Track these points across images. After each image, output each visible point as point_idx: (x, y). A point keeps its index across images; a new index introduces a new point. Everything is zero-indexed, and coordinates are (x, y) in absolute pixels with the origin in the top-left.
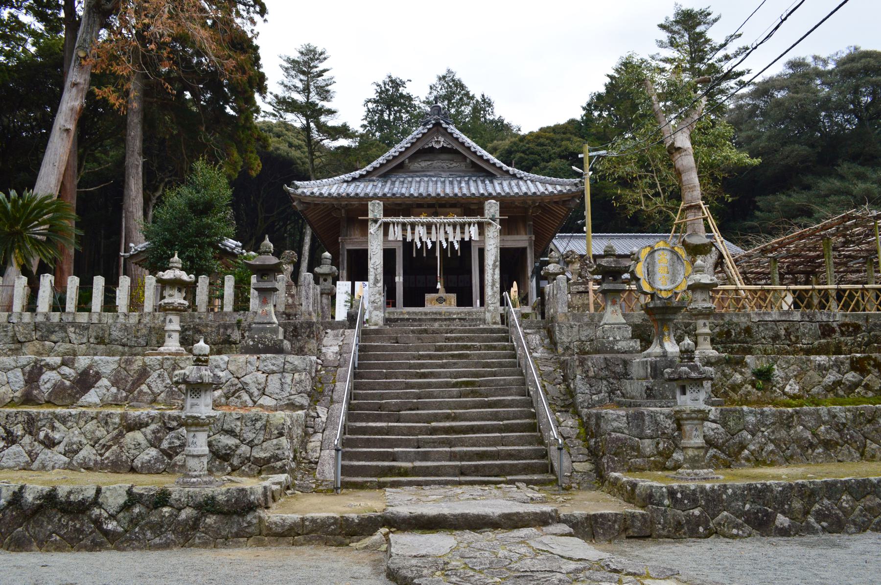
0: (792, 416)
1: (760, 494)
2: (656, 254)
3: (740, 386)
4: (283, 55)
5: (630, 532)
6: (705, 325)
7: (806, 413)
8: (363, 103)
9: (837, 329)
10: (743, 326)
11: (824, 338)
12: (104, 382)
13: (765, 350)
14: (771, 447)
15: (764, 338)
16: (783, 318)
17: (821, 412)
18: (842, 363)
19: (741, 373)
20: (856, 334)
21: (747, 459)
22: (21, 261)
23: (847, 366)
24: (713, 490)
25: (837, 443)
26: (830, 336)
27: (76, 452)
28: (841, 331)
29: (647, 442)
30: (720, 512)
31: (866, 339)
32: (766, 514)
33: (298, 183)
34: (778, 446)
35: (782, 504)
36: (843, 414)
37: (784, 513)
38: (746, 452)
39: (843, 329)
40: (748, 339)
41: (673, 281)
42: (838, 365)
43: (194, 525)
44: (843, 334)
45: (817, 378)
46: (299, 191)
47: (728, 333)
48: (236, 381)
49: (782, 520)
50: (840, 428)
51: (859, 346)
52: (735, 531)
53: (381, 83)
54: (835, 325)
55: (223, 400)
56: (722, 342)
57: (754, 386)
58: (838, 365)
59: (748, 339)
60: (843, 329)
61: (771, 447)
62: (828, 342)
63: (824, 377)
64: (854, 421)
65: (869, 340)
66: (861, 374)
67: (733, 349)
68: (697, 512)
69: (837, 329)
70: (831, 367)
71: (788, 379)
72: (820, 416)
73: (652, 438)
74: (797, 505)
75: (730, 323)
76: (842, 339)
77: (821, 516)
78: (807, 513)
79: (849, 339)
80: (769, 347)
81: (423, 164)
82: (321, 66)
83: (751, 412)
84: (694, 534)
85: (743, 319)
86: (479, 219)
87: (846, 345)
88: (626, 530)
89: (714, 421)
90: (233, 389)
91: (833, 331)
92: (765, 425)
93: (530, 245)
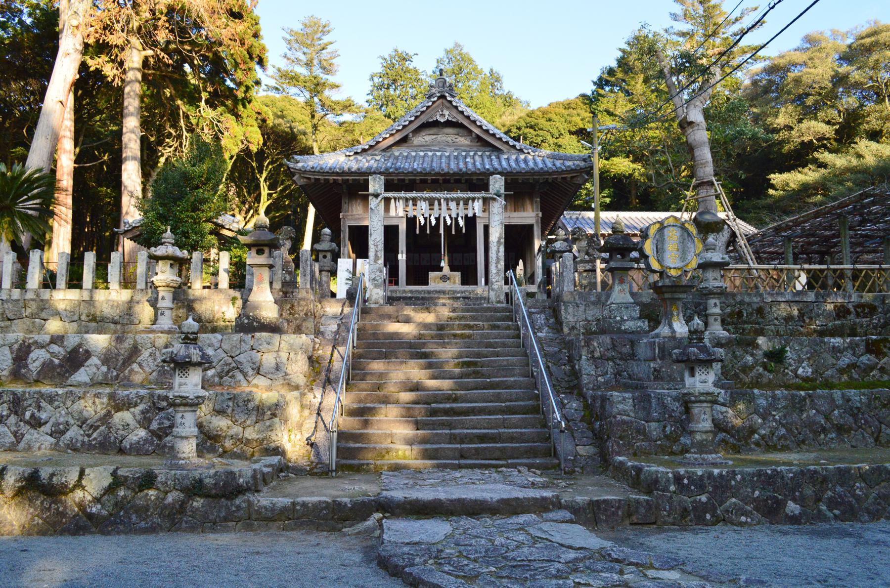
0: (804, 399)
1: (769, 480)
2: (666, 231)
3: (752, 368)
4: (286, 27)
5: (634, 519)
6: (715, 305)
7: (820, 397)
8: (368, 77)
9: (852, 310)
10: (755, 306)
11: (839, 319)
12: (94, 360)
13: (778, 331)
14: (783, 431)
15: (777, 319)
16: (797, 299)
17: (835, 396)
18: (857, 345)
19: (752, 355)
20: (872, 316)
21: (757, 444)
22: (11, 237)
23: (862, 348)
24: (721, 475)
25: (851, 429)
26: (844, 317)
27: (63, 433)
28: (857, 312)
29: (653, 425)
30: (727, 498)
31: (882, 321)
32: (777, 501)
33: (297, 157)
34: (789, 430)
35: (793, 490)
36: (857, 398)
37: (794, 500)
38: (756, 436)
39: (859, 310)
40: (761, 320)
41: (683, 259)
42: (853, 347)
43: (181, 508)
44: (858, 315)
45: (831, 361)
46: (300, 165)
47: (740, 314)
48: (230, 360)
49: (792, 507)
50: (855, 412)
51: (875, 327)
52: (743, 519)
53: (387, 57)
54: (850, 306)
55: (217, 379)
56: (733, 323)
57: (765, 368)
58: (853, 347)
59: (761, 320)
60: (859, 310)
61: (783, 431)
62: (843, 324)
63: (838, 359)
64: (869, 405)
65: (885, 322)
66: (877, 357)
67: (744, 330)
68: (704, 498)
69: (852, 310)
70: (845, 349)
71: (800, 361)
72: (833, 400)
73: (658, 421)
74: (809, 491)
75: (742, 303)
76: (858, 320)
77: (832, 504)
78: (818, 500)
79: (865, 321)
80: (782, 329)
81: (428, 138)
82: (326, 39)
83: (762, 395)
84: (700, 520)
85: (755, 299)
86: (483, 194)
87: (862, 326)
88: (630, 515)
89: (723, 405)
90: (226, 368)
91: (848, 312)
92: (776, 409)
93: (537, 222)
